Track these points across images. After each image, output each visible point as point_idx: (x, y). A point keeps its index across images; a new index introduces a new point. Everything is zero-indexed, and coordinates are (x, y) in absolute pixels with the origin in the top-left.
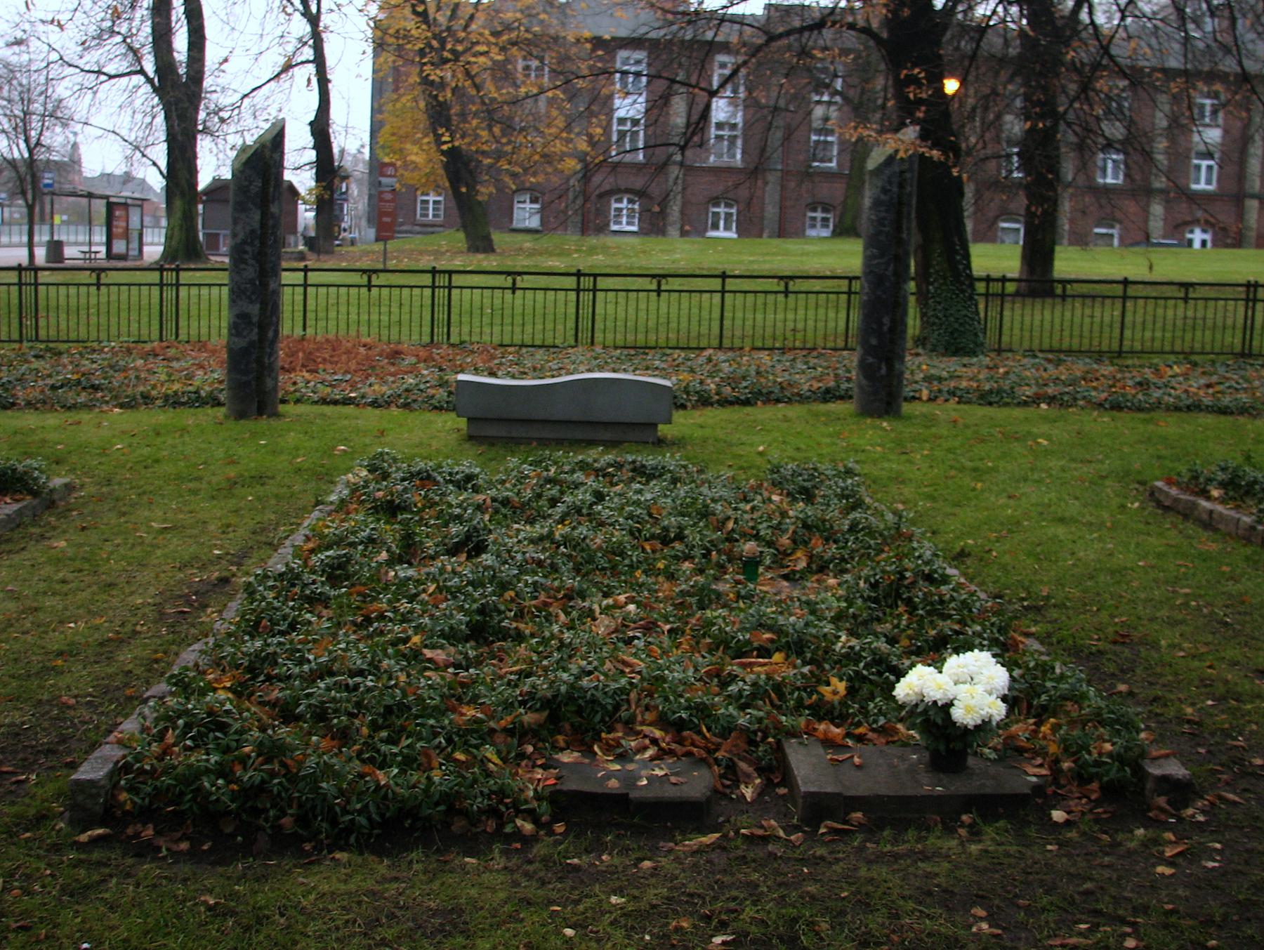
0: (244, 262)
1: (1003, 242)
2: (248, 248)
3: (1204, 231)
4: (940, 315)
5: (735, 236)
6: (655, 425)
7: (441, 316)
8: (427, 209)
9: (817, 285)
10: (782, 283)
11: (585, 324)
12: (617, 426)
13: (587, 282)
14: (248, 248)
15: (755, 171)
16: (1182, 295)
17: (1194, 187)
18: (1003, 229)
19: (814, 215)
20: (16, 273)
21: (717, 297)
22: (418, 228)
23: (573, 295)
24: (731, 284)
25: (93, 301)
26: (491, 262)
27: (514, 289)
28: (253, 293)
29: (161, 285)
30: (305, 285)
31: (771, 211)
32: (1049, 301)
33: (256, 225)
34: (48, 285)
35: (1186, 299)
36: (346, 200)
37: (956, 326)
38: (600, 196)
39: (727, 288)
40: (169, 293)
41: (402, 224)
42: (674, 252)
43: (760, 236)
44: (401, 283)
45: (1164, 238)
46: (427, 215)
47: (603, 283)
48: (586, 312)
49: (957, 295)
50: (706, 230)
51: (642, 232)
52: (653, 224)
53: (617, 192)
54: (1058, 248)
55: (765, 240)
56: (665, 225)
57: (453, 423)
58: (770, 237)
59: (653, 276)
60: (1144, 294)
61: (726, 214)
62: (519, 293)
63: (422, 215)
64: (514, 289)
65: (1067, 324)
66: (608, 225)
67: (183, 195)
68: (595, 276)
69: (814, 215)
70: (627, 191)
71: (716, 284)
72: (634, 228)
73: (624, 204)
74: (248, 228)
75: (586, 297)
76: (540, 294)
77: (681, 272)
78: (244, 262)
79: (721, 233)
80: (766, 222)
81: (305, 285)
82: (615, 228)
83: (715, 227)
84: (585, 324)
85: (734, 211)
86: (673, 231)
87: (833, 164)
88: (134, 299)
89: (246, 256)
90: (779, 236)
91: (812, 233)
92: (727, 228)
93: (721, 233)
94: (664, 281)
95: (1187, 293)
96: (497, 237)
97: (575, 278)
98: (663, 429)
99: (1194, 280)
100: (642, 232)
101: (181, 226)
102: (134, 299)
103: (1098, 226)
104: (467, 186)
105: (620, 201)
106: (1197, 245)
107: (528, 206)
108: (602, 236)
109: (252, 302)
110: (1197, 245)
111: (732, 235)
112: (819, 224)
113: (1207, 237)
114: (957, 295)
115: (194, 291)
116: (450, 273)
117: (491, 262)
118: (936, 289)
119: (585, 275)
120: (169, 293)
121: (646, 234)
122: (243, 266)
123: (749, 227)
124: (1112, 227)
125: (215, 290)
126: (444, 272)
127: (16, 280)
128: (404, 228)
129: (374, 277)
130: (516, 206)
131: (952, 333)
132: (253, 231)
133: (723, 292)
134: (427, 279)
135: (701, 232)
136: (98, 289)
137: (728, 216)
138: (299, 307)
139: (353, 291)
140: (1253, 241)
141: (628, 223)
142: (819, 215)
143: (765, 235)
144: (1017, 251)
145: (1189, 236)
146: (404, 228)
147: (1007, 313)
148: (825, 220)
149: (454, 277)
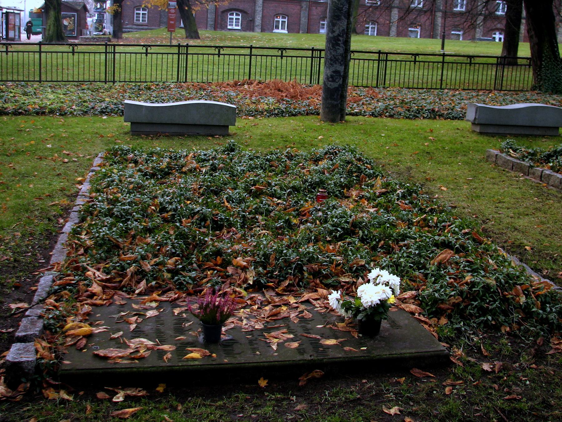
0: (338, 45)
1: (410, 37)
2: (341, 39)
3: (500, 34)
4: (549, 75)
5: (287, 32)
6: (228, 126)
8: (139, 17)
9: (399, 58)
10: (144, 48)
11: (381, 77)
12: (211, 125)
13: (383, 57)
14: (341, 39)
16: (5, 50)
17: (497, 13)
18: (411, 31)
19: (323, 23)
20: (311, 51)
22: (135, 27)
23: (176, 56)
24: (447, 59)
25: (71, 61)
27: (73, 52)
28: (342, 61)
30: (443, 62)
31: (304, 20)
32: (515, 67)
33: (345, 27)
36: (105, 12)
37: (556, 80)
38: (223, 12)
39: (42, 50)
41: (127, 24)
42: (257, 38)
43: (299, 33)
45: (483, 36)
46: (139, 20)
47: (391, 57)
48: (382, 72)
49: (557, 67)
50: (273, 29)
51: (244, 29)
52: (248, 26)
54: (520, 43)
55: (301, 34)
56: (254, 26)
57: (121, 124)
58: (303, 33)
59: (279, 49)
61: (282, 21)
62: (284, 58)
64: (73, 52)
65: (526, 79)
66: (227, 26)
68: (387, 54)
69: (323, 23)
70: (241, 11)
71: (247, 51)
72: (239, 28)
73: (234, 17)
74: (341, 29)
76: (237, 58)
78: (338, 45)
79: (280, 31)
80: (301, 26)
81: (251, 55)
82: (229, 27)
83: (277, 27)
84: (381, 77)
85: (286, 20)
86: (258, 29)
88: (269, 63)
89: (340, 42)
90: (307, 33)
92: (283, 28)
93: (280, 31)
97: (378, 55)
98: (232, 129)
99: (476, 54)
100: (244, 29)
101: (54, 25)
102: (154, 62)
103: (453, 31)
104: (187, 6)
105: (232, 14)
106: (497, 40)
108: (223, 31)
109: (341, 65)
110: (497, 40)
111: (285, 31)
113: (502, 37)
114: (557, 67)
115: (49, 55)
118: (546, 64)
120: (110, 56)
121: (244, 31)
122: (337, 47)
123: (293, 28)
124: (459, 31)
125: (97, 56)
126: (318, 50)
127: (441, 60)
128: (128, 26)
129: (221, 50)
131: (554, 84)
132: (343, 30)
134: (175, 50)
136: (282, 58)
139: (139, 56)
141: (236, 25)
143: (301, 32)
144: (324, 39)
145: (494, 36)
146: (128, 26)
147: (505, 73)
149: (117, 48)
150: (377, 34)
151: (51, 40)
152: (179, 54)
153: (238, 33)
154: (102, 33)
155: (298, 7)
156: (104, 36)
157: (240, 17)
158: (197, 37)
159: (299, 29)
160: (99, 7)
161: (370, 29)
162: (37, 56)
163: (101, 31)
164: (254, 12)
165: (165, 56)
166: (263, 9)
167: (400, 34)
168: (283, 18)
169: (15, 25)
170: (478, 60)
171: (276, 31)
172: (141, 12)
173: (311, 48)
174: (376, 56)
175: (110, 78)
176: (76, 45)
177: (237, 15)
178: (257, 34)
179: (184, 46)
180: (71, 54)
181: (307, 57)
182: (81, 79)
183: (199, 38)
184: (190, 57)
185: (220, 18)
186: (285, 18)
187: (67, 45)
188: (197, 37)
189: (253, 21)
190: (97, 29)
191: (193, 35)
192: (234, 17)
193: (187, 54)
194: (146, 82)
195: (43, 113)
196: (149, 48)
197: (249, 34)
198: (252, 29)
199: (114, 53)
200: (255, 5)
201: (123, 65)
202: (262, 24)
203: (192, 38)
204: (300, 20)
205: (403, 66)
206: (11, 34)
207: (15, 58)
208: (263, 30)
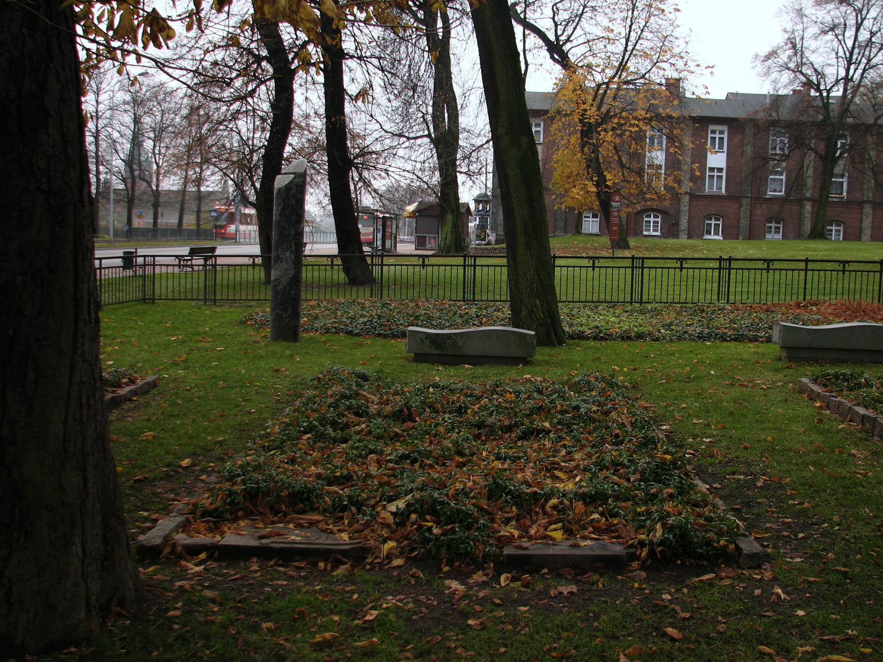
7: (724, 285)
9: (785, 265)
10: (329, 259)
13: (725, 264)
15: (732, 197)
21: (803, 273)
23: (629, 271)
26: (627, 253)
29: (464, 266)
31: (744, 222)
34: (482, 266)
35: (768, 270)
40: (470, 271)
44: (607, 265)
51: (664, 235)
52: (671, 230)
53: (647, 211)
55: (569, 235)
56: (678, 231)
60: (861, 269)
62: (684, 271)
63: (839, 231)
67: (452, 212)
70: (653, 210)
71: (802, 265)
72: (658, 234)
73: (652, 219)
75: (725, 273)
77: (749, 257)
79: (712, 237)
81: (806, 270)
82: (645, 233)
85: (720, 223)
87: (783, 193)
91: (768, 236)
92: (716, 233)
93: (712, 237)
94: (596, 261)
95: (681, 265)
96: (632, 242)
99: (849, 259)
100: (664, 235)
107: (591, 219)
111: (720, 238)
112: (773, 230)
116: (643, 259)
117: (627, 253)
119: (637, 258)
120: (470, 271)
123: (730, 233)
125: (454, 269)
126: (639, 258)
130: (584, 219)
133: (806, 270)
134: (716, 264)
135: (700, 237)
136: (593, 270)
137: (717, 226)
138: (802, 283)
140: (868, 237)
141: (654, 231)
142: (773, 225)
143: (740, 238)
148: (777, 228)
150: (844, 239)
151: (448, 251)
152: (633, 268)
153: (658, 241)
154: (484, 242)
155: (737, 205)
156: (489, 247)
157: (659, 220)
158: (627, 247)
159: (738, 234)
160: (481, 208)
161: (652, 224)
162: (461, 270)
163: (484, 239)
164: (678, 213)
165: (609, 270)
166: (690, 210)
167: (751, 236)
168: (837, 225)
169: (391, 233)
170: (777, 265)
171: (707, 237)
172: (713, 222)
173: (804, 258)
174: (716, 264)
175: (636, 297)
176: (427, 256)
177: (655, 216)
178: (683, 240)
179: (726, 260)
180: (764, 272)
181: (799, 270)
182: (615, 299)
183: (629, 248)
184: (646, 271)
185: (633, 221)
186: (719, 220)
187: (587, 258)
188: (627, 247)
189: (677, 224)
190: (478, 237)
191: (622, 244)
192: (652, 219)
193: (730, 269)
194: (686, 303)
195: (629, 338)
196: (596, 261)
197: (672, 241)
198: (676, 236)
199: (154, 265)
200: (679, 204)
201: (564, 282)
202: (688, 228)
203: (620, 247)
204: (739, 221)
205: (865, 277)
206: (388, 244)
207: (442, 274)
208: (690, 237)
